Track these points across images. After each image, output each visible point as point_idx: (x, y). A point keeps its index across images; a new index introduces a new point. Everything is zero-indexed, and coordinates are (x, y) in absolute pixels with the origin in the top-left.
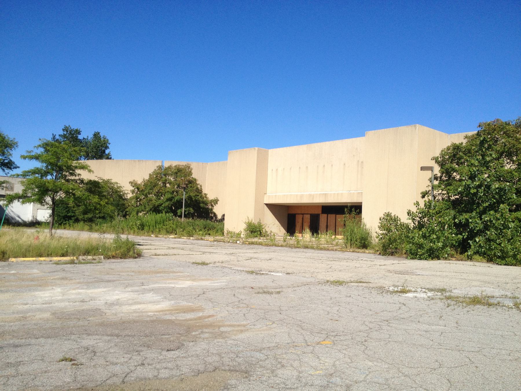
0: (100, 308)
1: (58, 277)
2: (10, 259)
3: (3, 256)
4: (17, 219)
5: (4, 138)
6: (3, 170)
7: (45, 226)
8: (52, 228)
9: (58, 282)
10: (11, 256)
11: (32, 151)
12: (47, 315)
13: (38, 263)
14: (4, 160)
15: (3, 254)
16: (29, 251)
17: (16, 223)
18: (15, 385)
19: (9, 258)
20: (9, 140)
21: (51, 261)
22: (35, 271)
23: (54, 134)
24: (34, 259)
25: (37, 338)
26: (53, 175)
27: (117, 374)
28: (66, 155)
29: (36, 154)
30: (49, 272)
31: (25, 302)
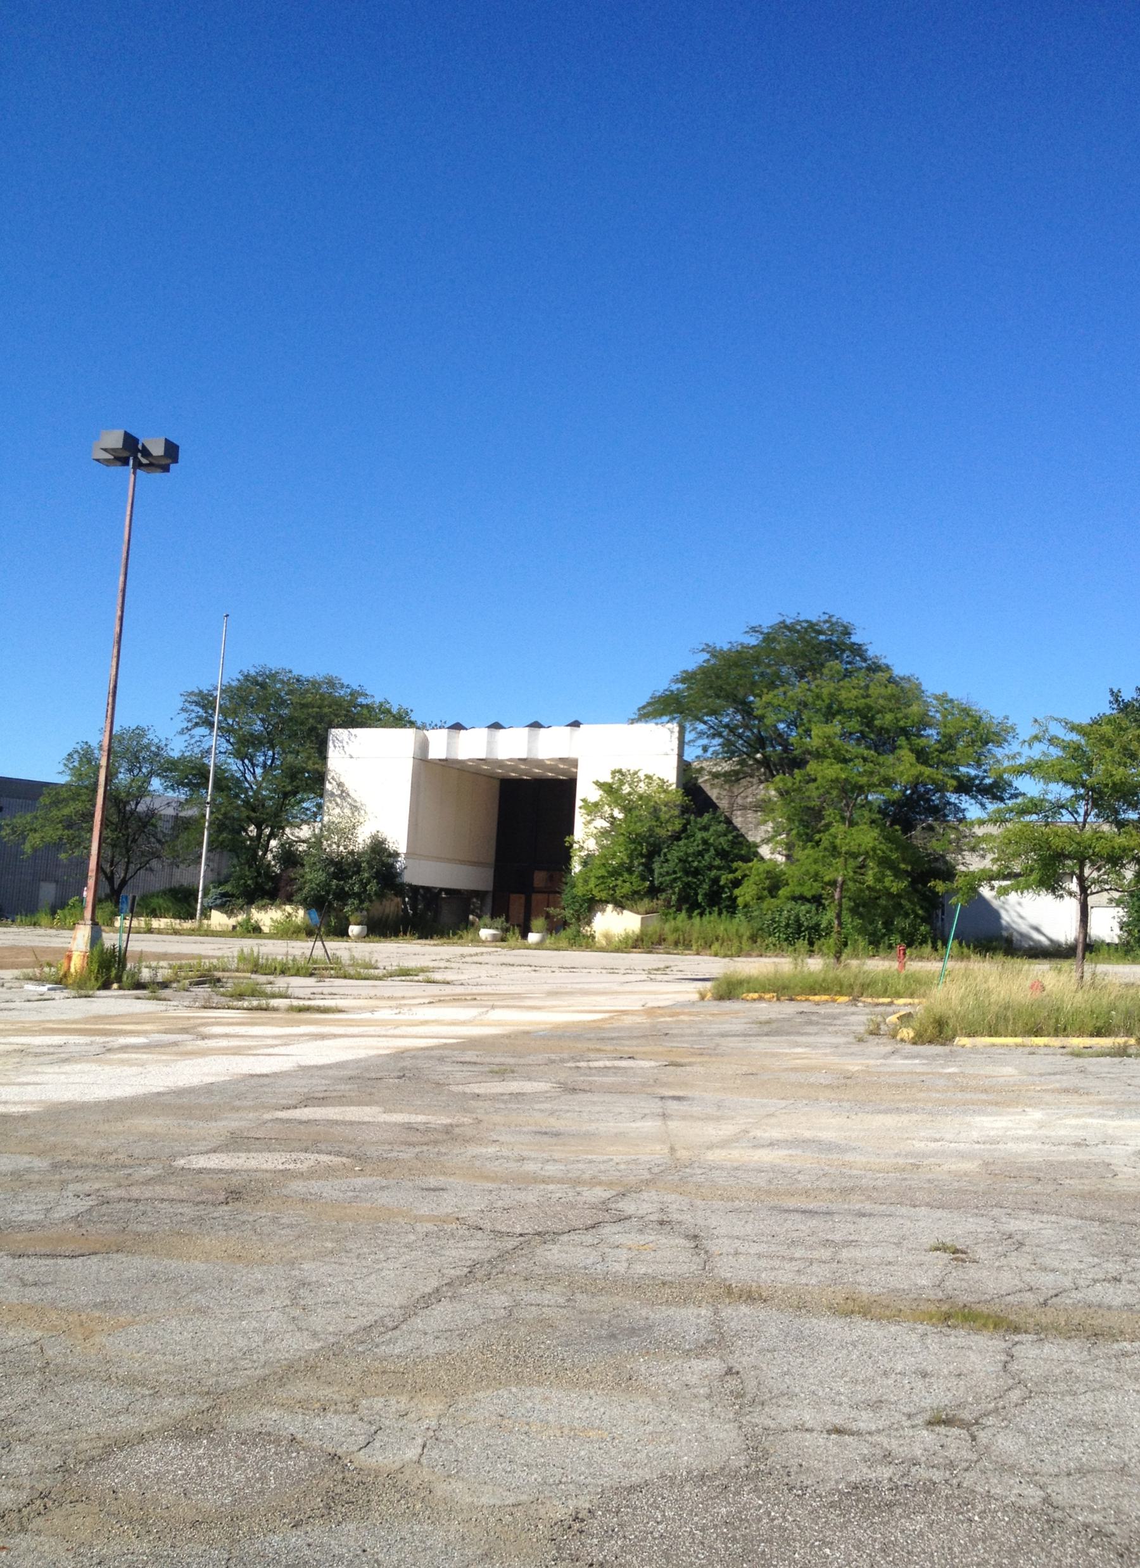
0: (1112, 1161)
1: (1058, 1085)
2: (957, 1038)
3: (941, 1032)
4: (1036, 936)
5: (978, 721)
6: (983, 805)
7: (1108, 953)
8: (1084, 958)
9: (1048, 1097)
10: (959, 1032)
11: (1018, 753)
12: (970, 1166)
13: (1027, 1050)
14: (984, 778)
15: (939, 1025)
16: (1006, 1019)
17: (1031, 948)
18: (817, 1276)
19: (954, 1037)
20: (993, 723)
21: (1064, 1047)
22: (1009, 1070)
23: (1115, 690)
24: (1019, 1040)
25: (915, 1206)
26: (1077, 812)
27: (1038, 1289)
28: (1108, 753)
29: (1028, 760)
30: (1041, 1075)
31: (938, 1136)
